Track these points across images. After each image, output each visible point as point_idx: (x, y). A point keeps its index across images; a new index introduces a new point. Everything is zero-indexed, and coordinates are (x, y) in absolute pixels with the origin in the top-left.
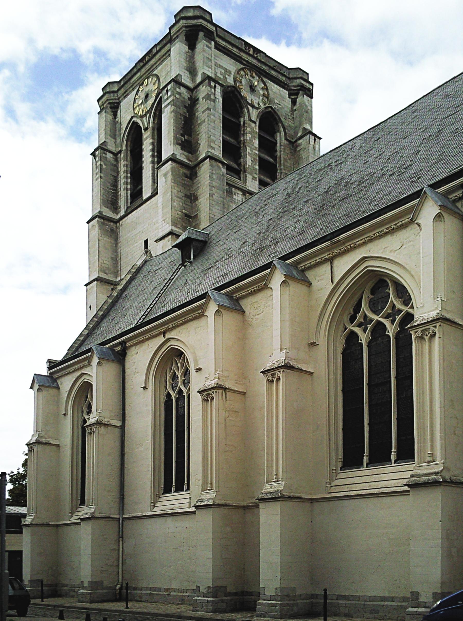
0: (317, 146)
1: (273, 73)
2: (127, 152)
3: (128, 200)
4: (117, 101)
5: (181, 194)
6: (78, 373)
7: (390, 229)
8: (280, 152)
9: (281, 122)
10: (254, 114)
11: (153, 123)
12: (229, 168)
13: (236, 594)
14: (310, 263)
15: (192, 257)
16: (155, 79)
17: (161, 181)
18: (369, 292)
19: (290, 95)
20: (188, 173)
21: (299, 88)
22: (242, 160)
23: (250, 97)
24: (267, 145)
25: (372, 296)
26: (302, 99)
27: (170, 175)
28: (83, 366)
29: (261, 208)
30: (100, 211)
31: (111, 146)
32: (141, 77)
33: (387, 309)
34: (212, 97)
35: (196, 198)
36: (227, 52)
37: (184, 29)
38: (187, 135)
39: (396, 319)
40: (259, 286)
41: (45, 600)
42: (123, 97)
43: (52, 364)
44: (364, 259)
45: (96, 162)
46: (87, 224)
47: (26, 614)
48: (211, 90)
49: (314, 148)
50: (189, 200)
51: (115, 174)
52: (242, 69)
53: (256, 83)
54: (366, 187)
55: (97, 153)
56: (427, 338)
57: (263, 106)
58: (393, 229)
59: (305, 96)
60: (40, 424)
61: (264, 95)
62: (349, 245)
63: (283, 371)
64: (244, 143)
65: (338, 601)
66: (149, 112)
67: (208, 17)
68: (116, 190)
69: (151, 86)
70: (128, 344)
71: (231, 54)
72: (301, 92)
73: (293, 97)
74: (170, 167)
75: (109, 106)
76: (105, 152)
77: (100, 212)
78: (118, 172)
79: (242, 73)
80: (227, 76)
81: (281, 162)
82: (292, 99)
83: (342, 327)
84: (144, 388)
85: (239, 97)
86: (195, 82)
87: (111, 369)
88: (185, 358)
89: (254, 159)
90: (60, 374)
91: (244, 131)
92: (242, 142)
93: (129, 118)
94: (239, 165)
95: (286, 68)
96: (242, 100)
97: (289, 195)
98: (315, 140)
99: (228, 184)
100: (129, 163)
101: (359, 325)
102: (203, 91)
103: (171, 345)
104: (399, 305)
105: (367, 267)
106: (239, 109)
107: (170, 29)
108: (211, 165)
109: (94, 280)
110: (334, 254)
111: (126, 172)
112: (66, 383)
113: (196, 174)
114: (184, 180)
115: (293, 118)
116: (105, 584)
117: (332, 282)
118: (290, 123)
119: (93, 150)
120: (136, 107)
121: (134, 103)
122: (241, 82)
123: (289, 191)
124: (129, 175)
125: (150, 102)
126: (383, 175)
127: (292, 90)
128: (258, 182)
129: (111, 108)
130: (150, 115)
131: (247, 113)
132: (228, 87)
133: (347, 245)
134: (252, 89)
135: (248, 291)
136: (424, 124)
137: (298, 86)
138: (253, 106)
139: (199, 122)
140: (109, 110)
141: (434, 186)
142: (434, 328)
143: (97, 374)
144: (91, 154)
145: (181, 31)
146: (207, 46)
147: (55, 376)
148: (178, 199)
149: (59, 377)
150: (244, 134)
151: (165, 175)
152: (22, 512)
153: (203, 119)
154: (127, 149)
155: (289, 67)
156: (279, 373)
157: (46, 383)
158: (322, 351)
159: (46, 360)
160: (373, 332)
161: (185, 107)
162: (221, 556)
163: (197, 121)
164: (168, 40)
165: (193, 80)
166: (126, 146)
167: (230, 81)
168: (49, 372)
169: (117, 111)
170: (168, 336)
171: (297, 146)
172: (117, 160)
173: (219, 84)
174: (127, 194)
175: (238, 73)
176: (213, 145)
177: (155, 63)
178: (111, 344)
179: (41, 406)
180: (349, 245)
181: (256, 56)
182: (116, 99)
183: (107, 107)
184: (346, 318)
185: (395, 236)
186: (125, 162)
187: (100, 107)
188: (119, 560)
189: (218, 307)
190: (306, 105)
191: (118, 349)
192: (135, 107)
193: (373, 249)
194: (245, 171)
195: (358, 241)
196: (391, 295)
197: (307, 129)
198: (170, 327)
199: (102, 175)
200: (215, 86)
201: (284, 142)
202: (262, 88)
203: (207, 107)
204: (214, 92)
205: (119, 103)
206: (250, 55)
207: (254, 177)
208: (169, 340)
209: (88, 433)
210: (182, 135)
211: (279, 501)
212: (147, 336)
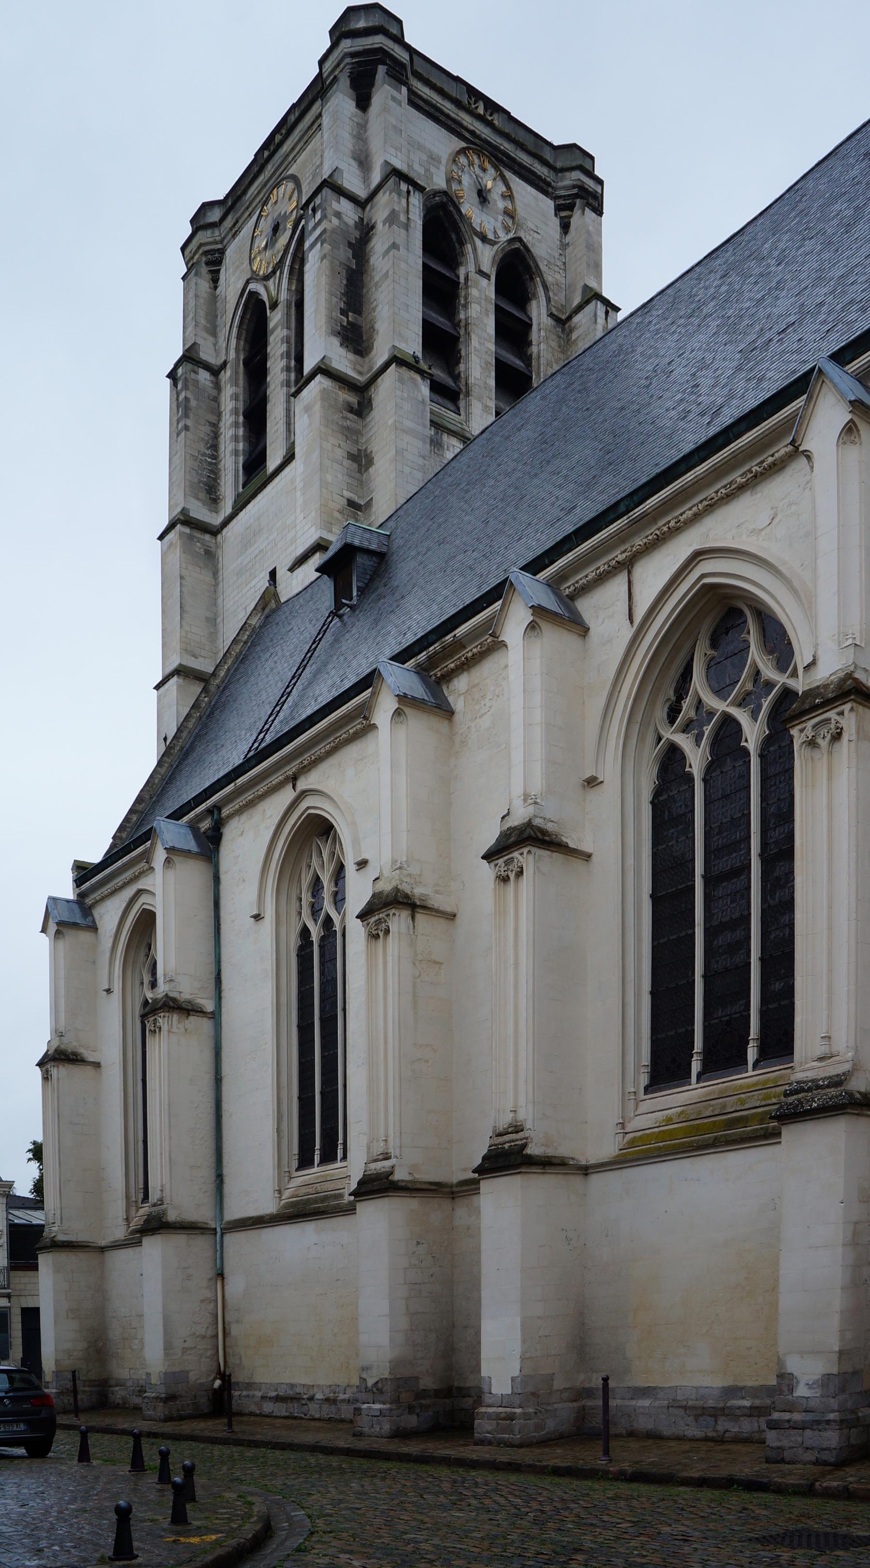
1: (524, 159)
2: (237, 365)
3: (238, 477)
4: (220, 246)
5: (340, 454)
7: (749, 476)
12: (436, 388)
13: (437, 1393)
14: (586, 576)
15: (355, 593)
16: (291, 185)
17: (301, 424)
18: (708, 642)
19: (558, 209)
20: (353, 399)
21: (575, 191)
22: (462, 367)
24: (513, 332)
26: (581, 218)
27: (317, 407)
28: (140, 873)
30: (184, 509)
31: (206, 354)
32: (265, 185)
33: (745, 682)
34: (403, 218)
35: (370, 462)
36: (432, 111)
37: (348, 60)
38: (354, 312)
40: (481, 644)
42: (230, 235)
43: (83, 872)
44: (698, 556)
45: (178, 394)
46: (159, 542)
47: (49, 1451)
48: (400, 200)
50: (355, 465)
51: (213, 419)
52: (462, 151)
53: (489, 184)
55: (180, 371)
56: (823, 743)
57: (504, 237)
58: (755, 476)
60: (62, 1016)
62: (664, 525)
63: (529, 852)
64: (467, 325)
66: (280, 265)
67: (394, 31)
69: (284, 202)
70: (225, 812)
71: (442, 118)
72: (578, 201)
73: (563, 214)
74: (318, 389)
75: (204, 259)
76: (196, 368)
77: (184, 511)
78: (219, 415)
79: (463, 160)
80: (433, 169)
81: (539, 368)
83: (650, 738)
84: (257, 917)
85: (456, 216)
86: (369, 185)
87: (193, 873)
88: (336, 839)
90: (96, 895)
91: (466, 298)
92: (462, 324)
93: (240, 285)
94: (456, 377)
95: (550, 144)
96: (461, 225)
98: (607, 313)
99: (433, 423)
100: (240, 390)
101: (686, 729)
103: (308, 808)
104: (769, 672)
105: (703, 576)
107: (321, 63)
108: (401, 380)
110: (634, 549)
111: (235, 411)
112: (110, 914)
113: (370, 401)
114: (346, 418)
115: (564, 263)
116: (193, 1377)
117: (632, 622)
118: (558, 276)
119: (172, 366)
120: (255, 258)
122: (460, 182)
124: (241, 419)
125: (283, 240)
127: (560, 197)
130: (282, 273)
131: (472, 256)
132: (436, 193)
133: (661, 523)
134: (483, 196)
135: (459, 658)
137: (574, 187)
138: (484, 239)
139: (377, 279)
140: (204, 269)
142: (837, 718)
143: (168, 888)
144: (168, 376)
145: (342, 66)
146: (394, 99)
147: (89, 901)
149: (97, 902)
152: (35, 1222)
153: (384, 271)
155: (556, 144)
156: (520, 857)
157: (69, 921)
158: (608, 798)
160: (716, 742)
161: (350, 245)
162: (407, 1308)
163: (372, 278)
164: (318, 91)
165: (366, 179)
167: (439, 182)
169: (218, 271)
171: (571, 331)
172: (217, 386)
174: (236, 463)
175: (454, 161)
177: (293, 149)
178: (192, 814)
179: (62, 974)
180: (664, 525)
181: (490, 118)
182: (216, 243)
183: (198, 262)
184: (661, 713)
185: (759, 495)
187: (187, 264)
188: (217, 1323)
189: (399, 702)
191: (205, 825)
192: (253, 256)
193: (716, 530)
194: (468, 394)
195: (684, 513)
196: (753, 648)
197: (591, 289)
198: (306, 762)
199: (189, 423)
200: (408, 192)
201: (545, 321)
202: (503, 196)
204: (405, 205)
205: (222, 252)
207: (486, 406)
208: (304, 794)
209: (150, 1030)
211: (520, 1173)
212: (262, 788)
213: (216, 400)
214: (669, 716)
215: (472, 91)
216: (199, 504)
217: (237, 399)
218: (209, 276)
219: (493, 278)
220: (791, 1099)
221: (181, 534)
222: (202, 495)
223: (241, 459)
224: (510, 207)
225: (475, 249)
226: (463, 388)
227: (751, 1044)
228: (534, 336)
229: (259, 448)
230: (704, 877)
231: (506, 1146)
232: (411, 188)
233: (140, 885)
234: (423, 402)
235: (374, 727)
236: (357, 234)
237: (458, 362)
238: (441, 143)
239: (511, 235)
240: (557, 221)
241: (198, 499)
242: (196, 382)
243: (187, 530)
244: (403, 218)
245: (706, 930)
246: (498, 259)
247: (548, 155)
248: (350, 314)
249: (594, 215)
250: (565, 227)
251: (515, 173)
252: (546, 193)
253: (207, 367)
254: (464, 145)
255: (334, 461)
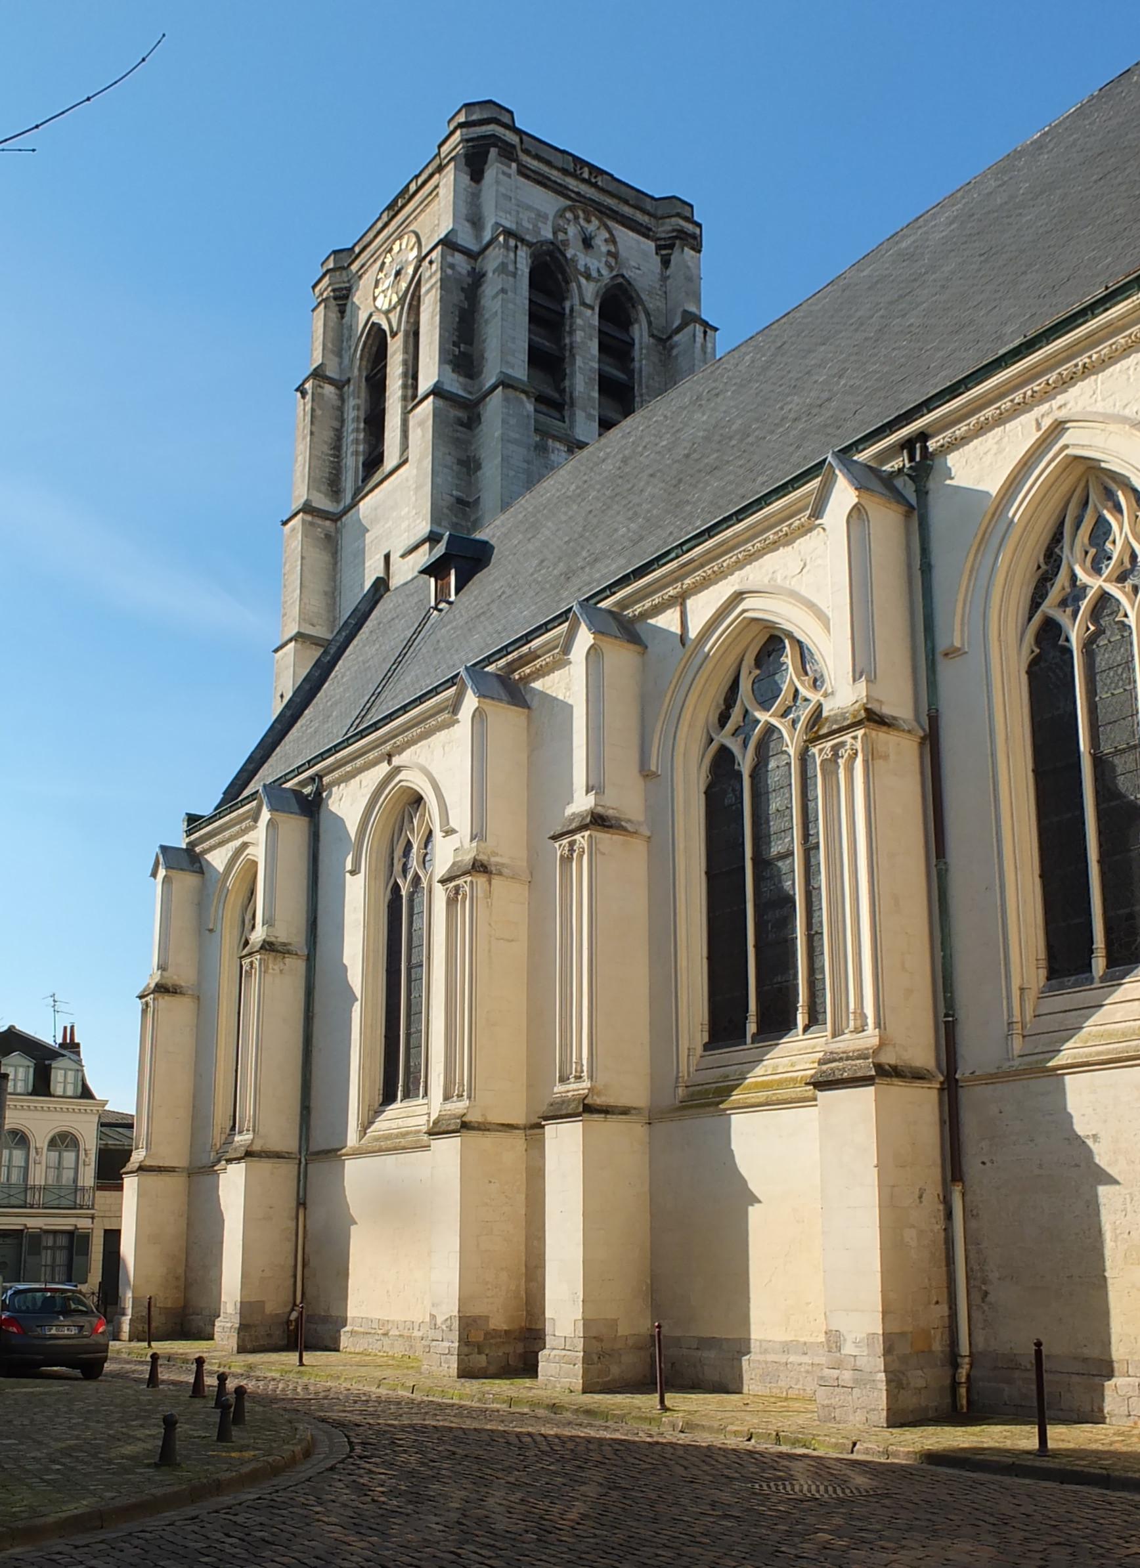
0: (709, 345)
1: (626, 210)
2: (360, 381)
5: (449, 460)
6: (237, 843)
8: (641, 361)
9: (642, 302)
10: (590, 291)
11: (408, 322)
12: (540, 399)
19: (659, 248)
22: (567, 383)
23: (583, 260)
24: (615, 348)
25: (758, 672)
29: (578, 487)
34: (511, 268)
35: (478, 467)
39: (1079, 608)
41: (153, 1344)
43: (193, 821)
44: (738, 597)
49: (704, 347)
50: (465, 470)
52: (570, 209)
54: (752, 444)
58: (786, 535)
59: (686, 249)
61: (609, 253)
64: (572, 348)
65: (699, 1353)
67: (506, 119)
68: (338, 457)
70: (326, 780)
71: (549, 183)
72: (678, 242)
73: (664, 252)
79: (569, 215)
80: (540, 225)
82: (662, 256)
85: (563, 261)
89: (590, 379)
90: (205, 845)
91: (571, 326)
92: (568, 347)
94: (562, 391)
95: (652, 198)
97: (625, 461)
98: (705, 333)
102: (494, 259)
106: (563, 284)
108: (506, 399)
109: (291, 640)
113: (479, 416)
118: (659, 304)
121: (376, 286)
123: (627, 452)
124: (362, 425)
126: (783, 419)
128: (597, 424)
129: (335, 298)
130: (402, 309)
132: (542, 243)
134: (587, 242)
136: (859, 314)
137: (674, 230)
138: (588, 277)
139: (487, 316)
141: (845, 453)
146: (504, 173)
148: (446, 470)
150: (571, 332)
151: (421, 424)
154: (360, 375)
155: (657, 196)
159: (183, 816)
161: (463, 289)
163: (483, 315)
166: (360, 369)
168: (187, 840)
169: (345, 305)
170: (396, 761)
171: (672, 348)
172: (342, 398)
173: (522, 240)
174: (357, 461)
176: (510, 359)
183: (327, 298)
186: (357, 401)
190: (688, 267)
194: (572, 405)
197: (690, 313)
200: (516, 247)
203: (500, 287)
206: (584, 181)
210: (454, 344)
213: (340, 409)
214: (719, 720)
215: (576, 159)
216: (322, 496)
217: (358, 409)
218: (337, 309)
219: (597, 309)
220: (824, 1067)
221: (303, 521)
222: (324, 488)
223: (361, 459)
224: (613, 250)
225: (579, 286)
226: (567, 399)
227: (800, 1010)
228: (636, 353)
229: (376, 453)
230: (753, 859)
231: (570, 1094)
232: (519, 244)
233: (245, 838)
234: (528, 416)
235: (457, 721)
236: (470, 280)
237: (563, 379)
238: (547, 202)
239: (614, 273)
240: (658, 259)
241: (320, 491)
242: (322, 395)
243: (309, 518)
244: (511, 268)
245: (756, 906)
246: (601, 293)
247: (649, 206)
248: (462, 345)
249: (692, 253)
250: (666, 262)
251: (618, 222)
252: (647, 237)
253: (331, 381)
254: (569, 203)
255: (446, 466)
